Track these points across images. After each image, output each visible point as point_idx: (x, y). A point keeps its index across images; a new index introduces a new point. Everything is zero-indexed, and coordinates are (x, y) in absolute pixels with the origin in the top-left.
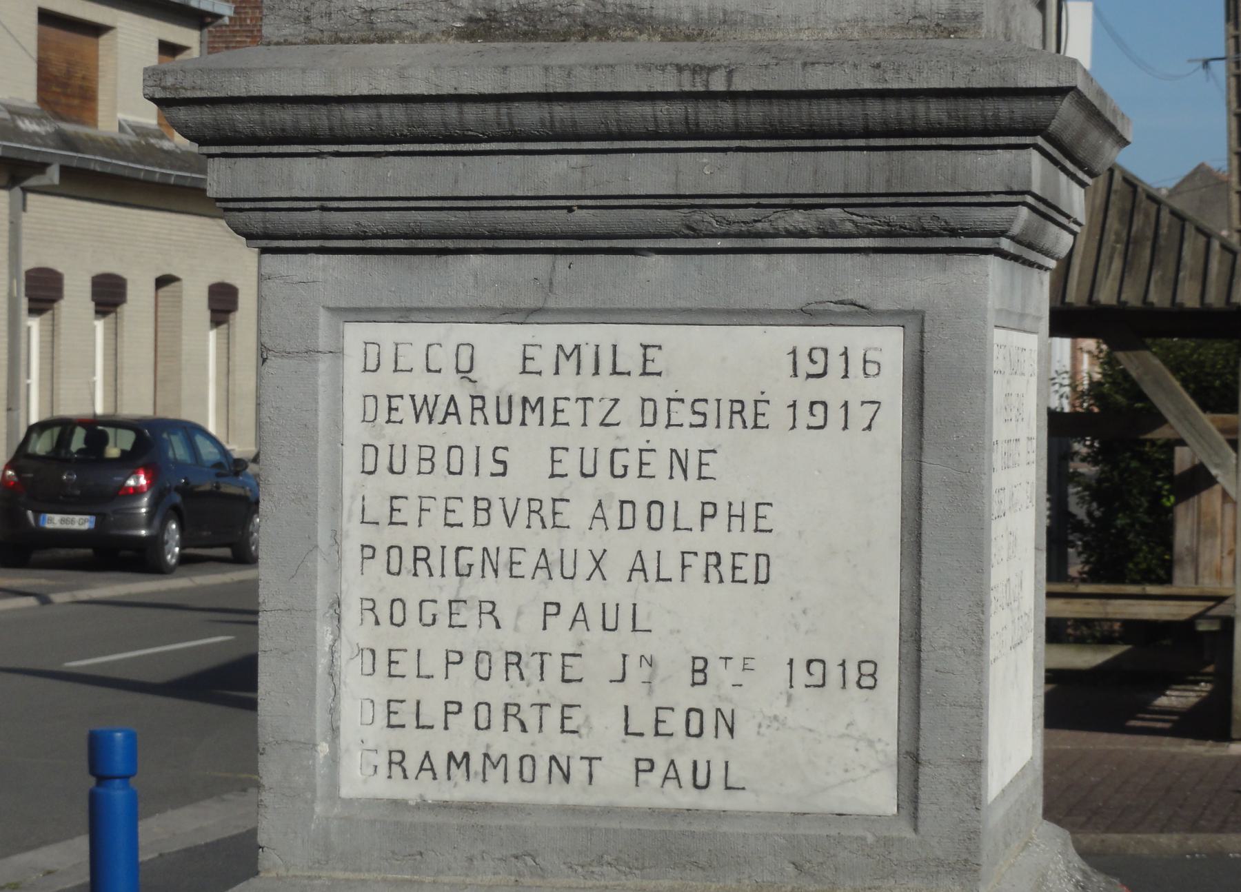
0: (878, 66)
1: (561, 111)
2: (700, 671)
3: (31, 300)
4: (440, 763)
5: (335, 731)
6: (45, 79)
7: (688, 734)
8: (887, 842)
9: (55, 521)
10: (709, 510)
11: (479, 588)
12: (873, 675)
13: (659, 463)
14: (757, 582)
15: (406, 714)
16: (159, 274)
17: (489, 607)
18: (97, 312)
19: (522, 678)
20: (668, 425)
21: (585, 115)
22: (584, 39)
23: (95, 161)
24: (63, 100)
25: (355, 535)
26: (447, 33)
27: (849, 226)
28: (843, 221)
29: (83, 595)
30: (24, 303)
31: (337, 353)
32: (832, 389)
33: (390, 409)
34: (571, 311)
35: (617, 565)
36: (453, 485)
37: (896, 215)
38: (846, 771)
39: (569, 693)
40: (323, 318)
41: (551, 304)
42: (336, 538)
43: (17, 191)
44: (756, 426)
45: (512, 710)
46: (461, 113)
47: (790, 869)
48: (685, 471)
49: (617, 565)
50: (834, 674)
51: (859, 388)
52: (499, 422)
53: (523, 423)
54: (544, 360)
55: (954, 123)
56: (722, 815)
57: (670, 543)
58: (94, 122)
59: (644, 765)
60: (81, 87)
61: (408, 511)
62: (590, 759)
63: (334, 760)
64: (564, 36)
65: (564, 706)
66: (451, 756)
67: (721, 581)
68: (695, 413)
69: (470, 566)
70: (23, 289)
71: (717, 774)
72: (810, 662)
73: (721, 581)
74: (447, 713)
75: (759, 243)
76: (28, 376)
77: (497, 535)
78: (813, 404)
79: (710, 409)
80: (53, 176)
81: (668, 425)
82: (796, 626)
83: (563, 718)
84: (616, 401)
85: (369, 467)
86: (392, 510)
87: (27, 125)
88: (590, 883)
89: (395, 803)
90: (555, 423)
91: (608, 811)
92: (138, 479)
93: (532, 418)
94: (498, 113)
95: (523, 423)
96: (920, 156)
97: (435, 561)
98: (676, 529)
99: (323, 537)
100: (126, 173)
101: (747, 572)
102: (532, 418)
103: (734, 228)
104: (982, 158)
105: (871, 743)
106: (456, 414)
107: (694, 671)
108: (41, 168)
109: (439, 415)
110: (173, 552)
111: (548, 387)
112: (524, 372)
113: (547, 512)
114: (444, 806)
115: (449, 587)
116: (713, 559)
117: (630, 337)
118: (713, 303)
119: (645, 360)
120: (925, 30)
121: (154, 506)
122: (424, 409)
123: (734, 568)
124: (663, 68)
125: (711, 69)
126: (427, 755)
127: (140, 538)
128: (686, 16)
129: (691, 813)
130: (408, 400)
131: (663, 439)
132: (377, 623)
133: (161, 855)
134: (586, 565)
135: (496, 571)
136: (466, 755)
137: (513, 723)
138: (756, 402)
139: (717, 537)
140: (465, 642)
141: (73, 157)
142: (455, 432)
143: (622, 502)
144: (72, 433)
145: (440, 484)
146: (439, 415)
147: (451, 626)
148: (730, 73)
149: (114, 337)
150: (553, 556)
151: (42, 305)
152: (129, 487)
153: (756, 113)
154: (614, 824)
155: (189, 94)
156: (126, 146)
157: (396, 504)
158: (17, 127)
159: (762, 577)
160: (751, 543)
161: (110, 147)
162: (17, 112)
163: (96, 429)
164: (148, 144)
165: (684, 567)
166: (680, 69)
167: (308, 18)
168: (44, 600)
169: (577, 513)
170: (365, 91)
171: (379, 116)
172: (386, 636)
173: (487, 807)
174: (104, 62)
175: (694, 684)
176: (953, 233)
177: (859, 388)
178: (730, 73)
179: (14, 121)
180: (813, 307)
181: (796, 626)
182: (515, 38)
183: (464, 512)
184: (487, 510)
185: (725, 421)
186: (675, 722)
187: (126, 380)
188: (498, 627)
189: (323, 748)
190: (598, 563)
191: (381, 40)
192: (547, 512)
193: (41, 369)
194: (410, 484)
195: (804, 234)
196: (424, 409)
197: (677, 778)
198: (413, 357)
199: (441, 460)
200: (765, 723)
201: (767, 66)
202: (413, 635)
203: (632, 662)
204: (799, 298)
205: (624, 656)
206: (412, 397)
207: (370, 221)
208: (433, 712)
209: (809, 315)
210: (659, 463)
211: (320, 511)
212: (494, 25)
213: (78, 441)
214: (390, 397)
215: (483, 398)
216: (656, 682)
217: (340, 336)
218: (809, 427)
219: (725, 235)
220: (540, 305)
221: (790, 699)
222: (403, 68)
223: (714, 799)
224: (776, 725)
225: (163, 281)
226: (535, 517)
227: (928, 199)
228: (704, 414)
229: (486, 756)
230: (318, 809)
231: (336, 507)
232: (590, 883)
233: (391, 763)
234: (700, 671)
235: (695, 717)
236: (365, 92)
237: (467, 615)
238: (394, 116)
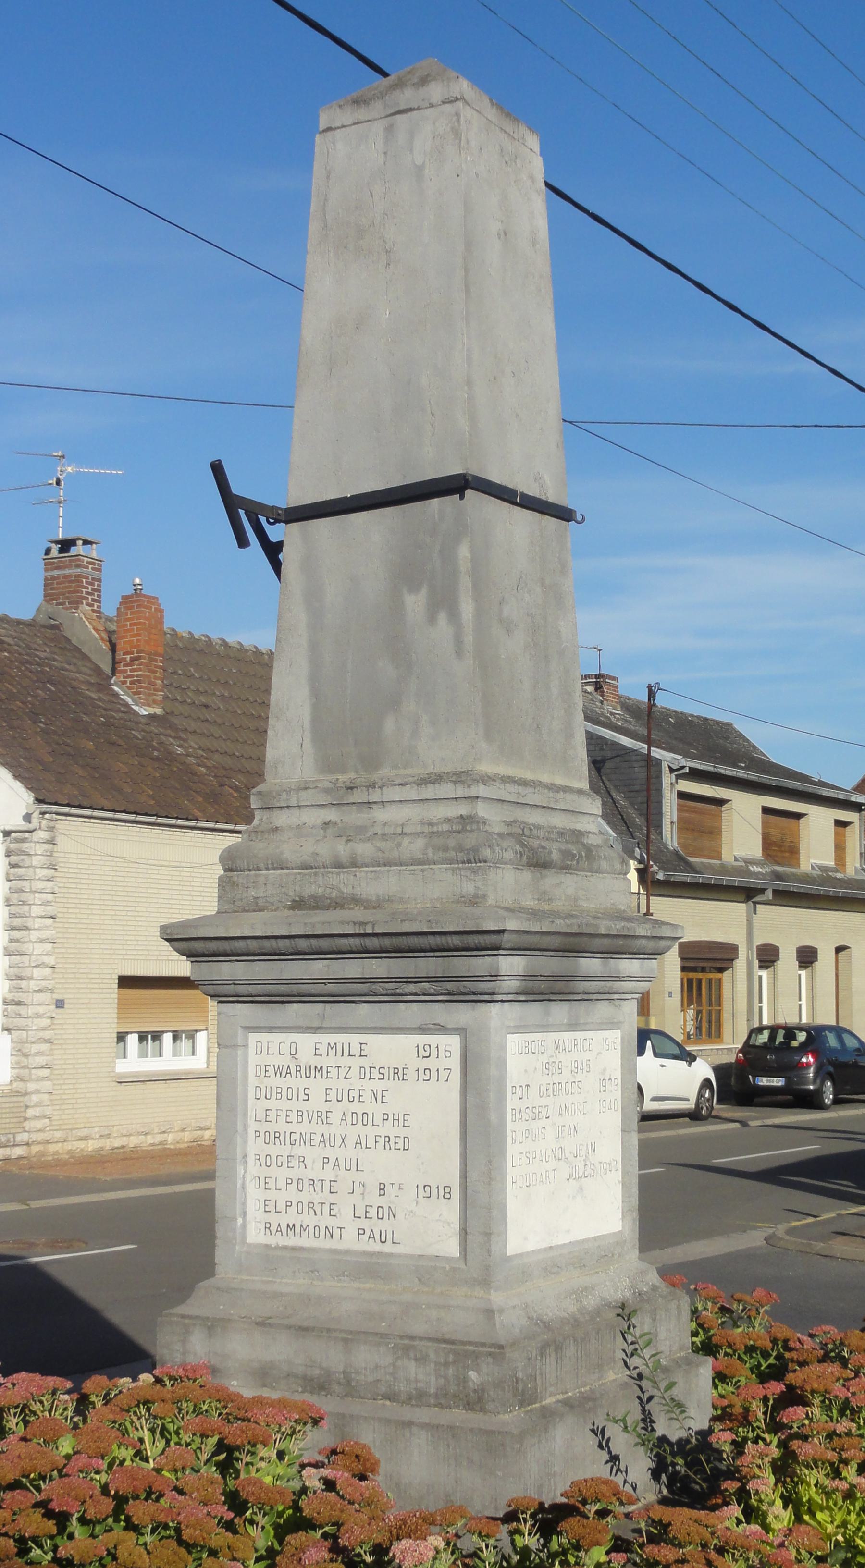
0: (429, 921)
1: (314, 942)
2: (382, 1189)
3: (760, 961)
4: (284, 1228)
5: (244, 1214)
6: (768, 843)
7: (378, 1218)
8: (454, 1270)
9: (764, 1081)
10: (386, 1117)
11: (299, 1150)
12: (449, 1193)
13: (366, 1095)
14: (404, 1149)
15: (271, 1207)
16: (837, 945)
17: (302, 1159)
18: (800, 966)
19: (315, 1191)
20: (370, 1079)
21: (324, 944)
22: (335, 909)
23: (793, 886)
24: (779, 854)
25: (253, 1126)
26: (284, 907)
27: (432, 991)
28: (430, 988)
29: (769, 1122)
30: (756, 963)
31: (246, 1046)
32: (431, 1063)
33: (266, 1071)
34: (330, 1028)
35: (351, 1141)
36: (288, 1105)
37: (450, 986)
38: (439, 1236)
39: (332, 1198)
40: (240, 1031)
41: (324, 1025)
42: (245, 1127)
43: (750, 903)
44: (403, 1080)
45: (311, 1205)
46: (277, 943)
47: (416, 1280)
48: (376, 1099)
49: (351, 1141)
50: (434, 1191)
51: (443, 1063)
52: (306, 1077)
53: (315, 1077)
54: (323, 1050)
55: (464, 946)
56: (391, 1255)
57: (371, 1131)
58: (799, 866)
59: (361, 1232)
60: (790, 846)
61: (272, 1116)
62: (341, 1228)
63: (244, 1226)
64: (327, 908)
65: (331, 1204)
66: (288, 1225)
67: (390, 1149)
68: (380, 1073)
69: (295, 1141)
70: (755, 956)
71: (389, 1236)
72: (425, 1187)
73: (390, 1149)
74: (287, 1206)
75: (401, 998)
76: (761, 1001)
77: (305, 1128)
78: (425, 1069)
79: (386, 1071)
80: (769, 895)
81: (370, 1079)
82: (419, 1169)
83: (330, 1209)
84: (350, 1068)
85: (258, 1097)
86: (266, 1115)
87: (755, 869)
88: (339, 1285)
89: (267, 1246)
90: (327, 1078)
91: (347, 1252)
92: (808, 1058)
93: (318, 1075)
94: (291, 944)
95: (315, 1077)
96: (480, 959)
97: (282, 1138)
98: (373, 1125)
99: (240, 1128)
100: (813, 892)
101: (400, 1145)
102: (318, 1075)
103: (389, 992)
104: (480, 960)
105: (449, 1224)
106: (290, 1073)
107: (380, 1189)
108: (762, 891)
109: (284, 1074)
110: (828, 1098)
111: (324, 1062)
112: (315, 1055)
113: (324, 1117)
114: (285, 1248)
115: (286, 1150)
116: (387, 1139)
117: (355, 1039)
118: (386, 1025)
119: (361, 1050)
120: (465, 902)
121: (817, 1073)
122: (278, 1071)
123: (395, 1143)
124: (348, 923)
125: (365, 924)
126: (279, 1225)
127: (809, 1090)
128: (374, 898)
129: (380, 1254)
130: (272, 1066)
131: (368, 1085)
132: (261, 1165)
133: (664, 1266)
134: (339, 1141)
135: (305, 1143)
136: (294, 1225)
137: (311, 1211)
138: (403, 1069)
139: (389, 1129)
140: (295, 1173)
141: (781, 885)
142: (290, 1081)
143: (353, 1113)
144: (777, 1032)
145: (285, 1105)
146: (284, 1074)
147: (288, 1167)
148: (373, 926)
149: (812, 979)
150: (326, 1136)
151: (767, 964)
152: (803, 1063)
153: (387, 942)
154: (349, 1258)
155: (176, 937)
156: (815, 878)
157: (268, 1113)
158: (749, 870)
159: (406, 1148)
160: (403, 1132)
161: (806, 879)
162: (749, 862)
163: (790, 1032)
164: (828, 875)
165: (376, 1142)
166: (355, 923)
167: (234, 901)
168: (744, 1124)
169: (336, 1118)
170: (239, 935)
171: (247, 945)
172: (264, 1172)
173: (301, 1249)
174: (803, 833)
175: (380, 1195)
176: (474, 993)
177: (443, 1063)
178: (373, 926)
179: (748, 866)
180: (424, 1026)
181: (419, 1169)
182: (310, 909)
183: (293, 1117)
184: (302, 1116)
185: (391, 1078)
186: (373, 1212)
187: (818, 1003)
188: (306, 1168)
189: (240, 1221)
190: (343, 1140)
191: (260, 911)
192: (324, 1117)
193: (768, 998)
194: (273, 1104)
195: (416, 994)
196: (278, 1071)
197: (374, 1237)
198: (274, 1049)
199: (284, 1093)
200: (408, 1214)
201: (387, 922)
202: (274, 1171)
203: (357, 1184)
204: (417, 1023)
205: (353, 1182)
206: (274, 1066)
207: (251, 989)
208: (281, 1206)
209: (423, 1030)
210: (366, 1095)
211: (238, 1116)
212: (302, 903)
213: (780, 1039)
214: (266, 1066)
215: (300, 1066)
216: (365, 1194)
217: (247, 1039)
218: (424, 1080)
219: (386, 995)
220: (320, 1025)
221: (417, 1203)
222: (253, 924)
223: (388, 1248)
224: (412, 1214)
225: (839, 950)
226: (319, 1119)
227: (459, 979)
228: (383, 1074)
229: (301, 1226)
230: (237, 1248)
231: (245, 1114)
232: (339, 1285)
233: (266, 1228)
234: (382, 1189)
235: (381, 1210)
236: (239, 935)
237: (294, 1163)
238: (253, 945)
